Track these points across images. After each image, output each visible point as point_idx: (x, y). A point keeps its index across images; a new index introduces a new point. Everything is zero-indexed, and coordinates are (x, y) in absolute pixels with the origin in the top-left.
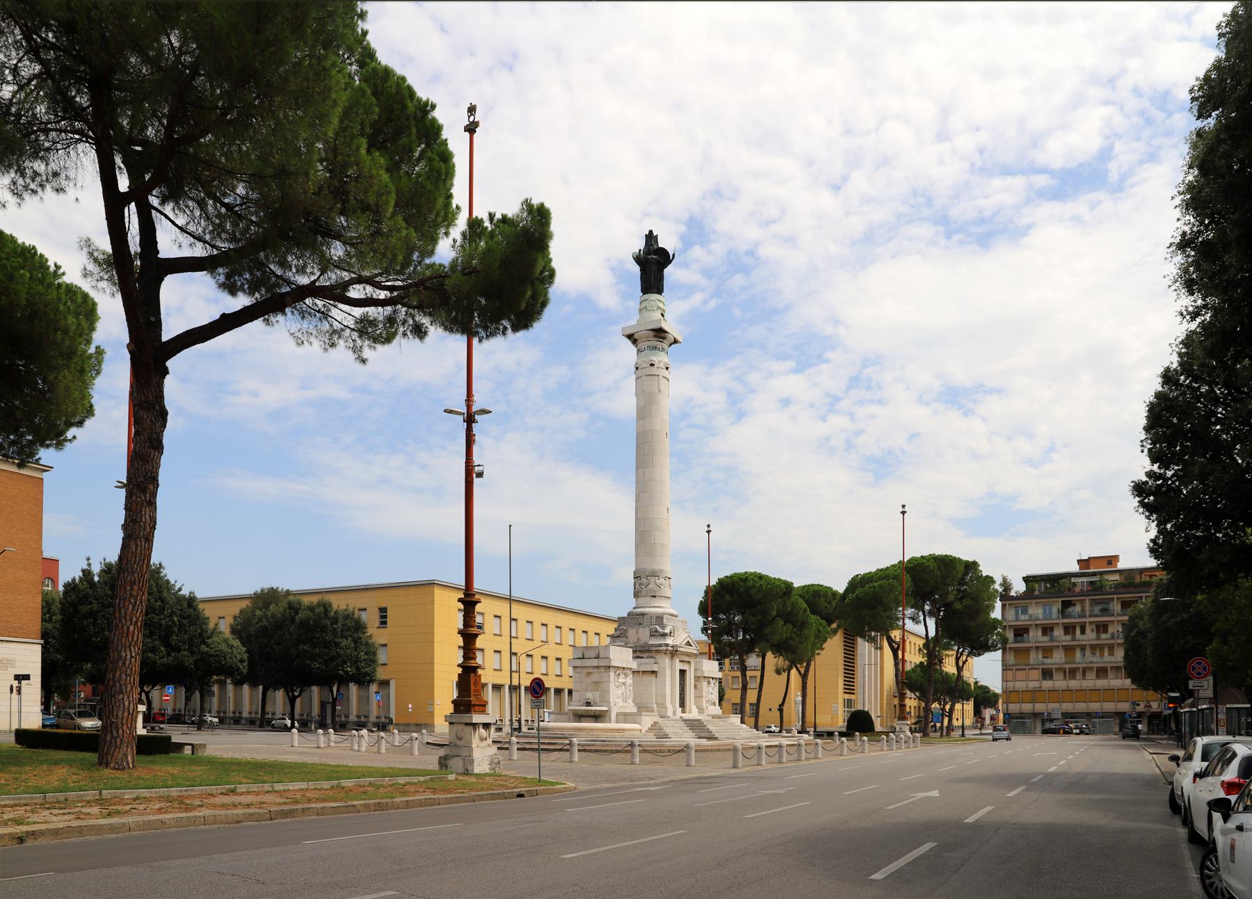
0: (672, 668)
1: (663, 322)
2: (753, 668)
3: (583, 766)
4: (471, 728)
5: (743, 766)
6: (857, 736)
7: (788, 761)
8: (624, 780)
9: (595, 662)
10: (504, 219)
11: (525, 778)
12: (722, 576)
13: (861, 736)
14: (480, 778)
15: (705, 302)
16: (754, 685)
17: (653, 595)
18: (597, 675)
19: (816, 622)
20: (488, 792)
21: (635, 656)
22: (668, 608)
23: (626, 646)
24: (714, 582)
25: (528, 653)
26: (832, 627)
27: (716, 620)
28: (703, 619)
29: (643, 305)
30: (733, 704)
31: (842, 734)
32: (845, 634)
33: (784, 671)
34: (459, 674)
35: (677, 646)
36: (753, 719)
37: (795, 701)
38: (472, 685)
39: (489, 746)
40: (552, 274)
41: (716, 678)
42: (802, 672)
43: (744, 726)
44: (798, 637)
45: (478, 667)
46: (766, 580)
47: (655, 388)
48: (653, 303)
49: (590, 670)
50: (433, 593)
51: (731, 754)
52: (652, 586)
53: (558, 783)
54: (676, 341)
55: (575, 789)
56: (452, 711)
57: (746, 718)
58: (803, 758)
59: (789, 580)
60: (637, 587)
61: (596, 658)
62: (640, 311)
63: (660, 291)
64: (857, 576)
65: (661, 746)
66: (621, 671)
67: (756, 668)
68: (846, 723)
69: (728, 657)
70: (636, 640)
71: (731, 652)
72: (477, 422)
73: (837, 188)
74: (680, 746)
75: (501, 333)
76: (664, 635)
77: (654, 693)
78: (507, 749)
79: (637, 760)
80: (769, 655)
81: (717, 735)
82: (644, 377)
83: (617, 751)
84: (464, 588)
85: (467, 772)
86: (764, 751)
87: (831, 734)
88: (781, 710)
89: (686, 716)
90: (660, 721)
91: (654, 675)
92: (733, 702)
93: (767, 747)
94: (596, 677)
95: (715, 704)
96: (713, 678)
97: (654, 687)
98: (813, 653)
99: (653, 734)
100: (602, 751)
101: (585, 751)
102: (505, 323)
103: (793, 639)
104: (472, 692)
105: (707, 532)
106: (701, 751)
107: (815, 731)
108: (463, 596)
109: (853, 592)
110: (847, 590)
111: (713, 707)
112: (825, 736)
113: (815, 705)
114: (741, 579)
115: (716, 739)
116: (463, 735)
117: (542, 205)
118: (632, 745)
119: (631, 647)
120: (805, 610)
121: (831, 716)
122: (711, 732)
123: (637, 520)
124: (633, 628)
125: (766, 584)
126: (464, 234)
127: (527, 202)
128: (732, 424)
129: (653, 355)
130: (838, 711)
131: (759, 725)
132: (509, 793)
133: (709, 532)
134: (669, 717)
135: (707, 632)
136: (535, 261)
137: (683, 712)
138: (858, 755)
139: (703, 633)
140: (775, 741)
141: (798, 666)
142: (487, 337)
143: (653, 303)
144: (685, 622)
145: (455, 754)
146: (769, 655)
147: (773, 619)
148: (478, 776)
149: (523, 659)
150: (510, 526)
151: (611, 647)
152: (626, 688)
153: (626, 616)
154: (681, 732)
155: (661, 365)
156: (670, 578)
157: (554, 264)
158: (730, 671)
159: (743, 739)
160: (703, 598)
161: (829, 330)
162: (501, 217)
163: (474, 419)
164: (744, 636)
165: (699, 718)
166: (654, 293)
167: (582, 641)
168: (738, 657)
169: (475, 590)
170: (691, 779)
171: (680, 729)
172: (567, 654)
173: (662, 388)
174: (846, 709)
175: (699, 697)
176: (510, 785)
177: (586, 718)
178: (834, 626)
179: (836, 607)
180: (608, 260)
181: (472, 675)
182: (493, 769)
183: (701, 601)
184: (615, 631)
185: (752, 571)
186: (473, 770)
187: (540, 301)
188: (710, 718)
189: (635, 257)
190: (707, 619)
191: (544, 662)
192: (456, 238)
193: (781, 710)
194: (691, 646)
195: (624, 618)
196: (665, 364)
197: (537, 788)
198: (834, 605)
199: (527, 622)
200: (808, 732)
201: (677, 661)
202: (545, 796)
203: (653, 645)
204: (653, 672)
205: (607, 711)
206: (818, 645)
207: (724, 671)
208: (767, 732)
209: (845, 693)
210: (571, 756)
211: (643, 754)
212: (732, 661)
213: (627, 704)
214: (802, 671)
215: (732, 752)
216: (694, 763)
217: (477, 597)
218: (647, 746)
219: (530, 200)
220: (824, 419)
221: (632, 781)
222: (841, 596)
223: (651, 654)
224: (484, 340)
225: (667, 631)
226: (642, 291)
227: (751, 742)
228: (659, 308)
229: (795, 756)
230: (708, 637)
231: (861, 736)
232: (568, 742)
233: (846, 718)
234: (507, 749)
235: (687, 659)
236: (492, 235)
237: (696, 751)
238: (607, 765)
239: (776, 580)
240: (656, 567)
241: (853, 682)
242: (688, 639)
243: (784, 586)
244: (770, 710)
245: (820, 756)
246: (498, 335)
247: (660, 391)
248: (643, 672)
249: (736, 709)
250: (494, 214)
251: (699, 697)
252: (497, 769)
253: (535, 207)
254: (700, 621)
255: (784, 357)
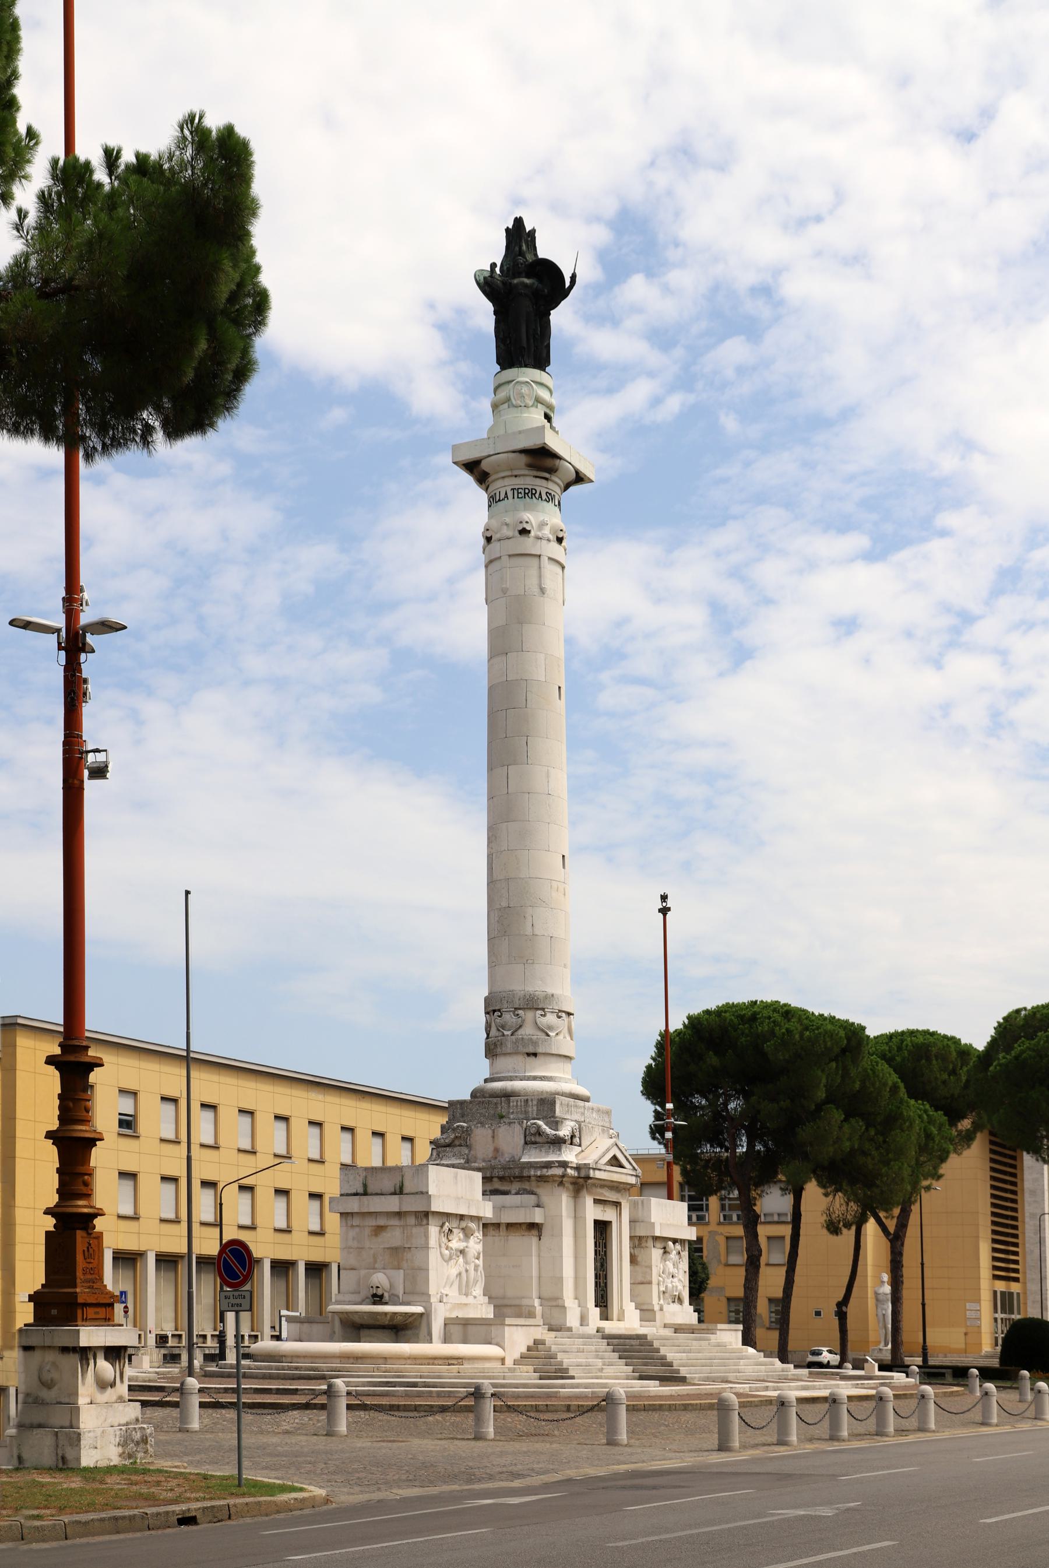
0: (578, 1218)
1: (548, 432)
2: (776, 1218)
3: (359, 1444)
4: (75, 1358)
5: (744, 1447)
6: (1023, 1378)
7: (855, 1436)
8: (451, 1477)
9: (392, 1204)
10: (143, 165)
11: (205, 1477)
12: (696, 1010)
13: (1033, 1380)
14: (94, 1479)
15: (656, 401)
16: (774, 1257)
17: (531, 1050)
18: (397, 1232)
19: (920, 1117)
20: (103, 1515)
21: (489, 1187)
22: (566, 1081)
23: (467, 1165)
24: (677, 1023)
25: (244, 1182)
26: (960, 1127)
27: (684, 1108)
28: (652, 1108)
29: (502, 394)
30: (729, 1299)
31: (987, 1374)
32: (992, 1142)
33: (848, 1226)
34: (48, 1234)
35: (587, 1167)
36: (775, 1335)
37: (876, 1294)
38: (79, 1257)
39: (120, 1399)
40: (261, 302)
41: (682, 1242)
42: (892, 1229)
43: (751, 1350)
44: (877, 1149)
45: (95, 1216)
46: (800, 1020)
47: (532, 583)
48: (525, 390)
49: (381, 1222)
50: (15, 1046)
51: (713, 1415)
52: (528, 1031)
53: (284, 1489)
54: (579, 478)
55: (327, 1501)
56: (31, 1320)
57: (759, 1333)
58: (891, 1429)
59: (855, 1019)
60: (494, 1032)
61: (395, 1193)
62: (495, 406)
63: (541, 361)
64: (1018, 1011)
65: (549, 1396)
66: (454, 1223)
67: (783, 1219)
68: (999, 1348)
69: (715, 1192)
70: (490, 1153)
71: (721, 1181)
72: (93, 651)
73: (967, 137)
74: (594, 1395)
75: (138, 439)
76: (557, 1142)
77: (535, 1273)
78: (175, 1405)
79: (490, 1430)
80: (812, 1190)
81: (684, 1372)
82: (505, 559)
83: (443, 1409)
84: (61, 1029)
85: (65, 1465)
86: (794, 1410)
87: (960, 1373)
88: (842, 1316)
89: (611, 1327)
90: (549, 1337)
91: (535, 1232)
92: (728, 1295)
93: (801, 1401)
94: (394, 1237)
95: (680, 1300)
96: (675, 1241)
97: (534, 1260)
98: (915, 1188)
99: (531, 1368)
100: (406, 1408)
101: (364, 1407)
102: (148, 416)
103: (864, 1153)
104: (79, 1274)
105: (660, 911)
106: (645, 1409)
107: (924, 1366)
108: (57, 1051)
109: (1008, 1049)
110: (993, 1044)
111: (676, 1307)
112: (949, 1378)
113: (923, 1305)
114: (741, 1017)
115: (683, 1380)
116: (55, 1375)
117: (229, 131)
118: (477, 1394)
119: (478, 1169)
120: (895, 1089)
121: (964, 1330)
122: (670, 1365)
123: (491, 882)
124: (483, 1124)
125: (800, 1028)
126: (43, 198)
127: (192, 121)
128: (721, 675)
129: (526, 509)
130: (979, 1319)
131: (789, 1348)
132: (158, 1514)
133: (664, 911)
134: (570, 1329)
135: (663, 1136)
136: (216, 267)
137: (605, 1316)
138: (1026, 1426)
139: (654, 1138)
140: (821, 1388)
141: (882, 1214)
142: (105, 448)
143: (525, 390)
144: (608, 1113)
145: (36, 1421)
146: (812, 1190)
147: (819, 1108)
148: (93, 1473)
149: (231, 1195)
150: (187, 893)
151: (433, 1170)
152: (466, 1263)
153: (468, 1097)
154: (599, 1363)
155: (546, 532)
156: (569, 1014)
157: (265, 279)
158: (720, 1223)
159: (747, 1381)
160: (653, 1059)
161: (948, 463)
162: (134, 160)
163: (84, 644)
164: (751, 1145)
165: (642, 1331)
166: (526, 366)
167: (371, 1156)
168: (736, 1192)
169: (87, 1034)
170: (615, 1476)
171: (597, 1357)
172: (331, 1185)
173: (548, 584)
174: (1000, 1315)
175: (641, 1282)
176: (164, 1495)
177: (372, 1332)
178: (965, 1124)
179: (967, 1081)
180: (431, 306)
181: (80, 1234)
182: (130, 1456)
183: (649, 1067)
184: (443, 1132)
185: (768, 998)
186: (78, 1459)
187: (232, 366)
188: (668, 1333)
189: (482, 280)
190: (663, 1106)
191: (281, 1202)
192: (24, 207)
193: (842, 1316)
194: (622, 1166)
195: (462, 1103)
196: (553, 530)
197: (231, 1501)
198: (964, 1078)
199: (310, 1123)
200: (904, 1368)
201: (589, 1201)
202: (248, 1520)
203: (531, 1165)
204: (534, 1227)
205: (421, 1315)
206: (928, 1168)
207: (708, 1224)
208: (811, 1365)
209: (996, 1277)
210: (331, 1420)
211: (502, 1416)
212: (727, 1202)
213: (470, 1300)
214: (891, 1225)
215: (715, 1412)
216: (625, 1437)
217: (91, 1053)
218: (517, 1396)
219: (201, 118)
220: (937, 664)
221: (469, 1481)
222: (979, 1057)
223: (526, 1186)
224: (97, 457)
225: (564, 1132)
226: (498, 362)
227: (767, 1389)
228: (538, 401)
229: (871, 1425)
230: (666, 1146)
231: (1033, 1380)
232: (325, 1387)
233: (1001, 1336)
234: (175, 1405)
235: (612, 1196)
236: (112, 199)
237: (631, 1409)
238: (416, 1442)
239: (825, 1019)
240: (537, 987)
241: (1016, 1253)
242: (615, 1151)
243: (842, 1033)
244: (818, 1314)
245: (932, 1426)
246: (133, 447)
247: (542, 591)
248: (509, 1226)
249: (737, 1312)
250: (119, 152)
251: (641, 1282)
252: (140, 1455)
253: (214, 134)
254: (646, 1111)
255: (844, 525)
